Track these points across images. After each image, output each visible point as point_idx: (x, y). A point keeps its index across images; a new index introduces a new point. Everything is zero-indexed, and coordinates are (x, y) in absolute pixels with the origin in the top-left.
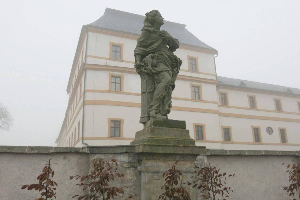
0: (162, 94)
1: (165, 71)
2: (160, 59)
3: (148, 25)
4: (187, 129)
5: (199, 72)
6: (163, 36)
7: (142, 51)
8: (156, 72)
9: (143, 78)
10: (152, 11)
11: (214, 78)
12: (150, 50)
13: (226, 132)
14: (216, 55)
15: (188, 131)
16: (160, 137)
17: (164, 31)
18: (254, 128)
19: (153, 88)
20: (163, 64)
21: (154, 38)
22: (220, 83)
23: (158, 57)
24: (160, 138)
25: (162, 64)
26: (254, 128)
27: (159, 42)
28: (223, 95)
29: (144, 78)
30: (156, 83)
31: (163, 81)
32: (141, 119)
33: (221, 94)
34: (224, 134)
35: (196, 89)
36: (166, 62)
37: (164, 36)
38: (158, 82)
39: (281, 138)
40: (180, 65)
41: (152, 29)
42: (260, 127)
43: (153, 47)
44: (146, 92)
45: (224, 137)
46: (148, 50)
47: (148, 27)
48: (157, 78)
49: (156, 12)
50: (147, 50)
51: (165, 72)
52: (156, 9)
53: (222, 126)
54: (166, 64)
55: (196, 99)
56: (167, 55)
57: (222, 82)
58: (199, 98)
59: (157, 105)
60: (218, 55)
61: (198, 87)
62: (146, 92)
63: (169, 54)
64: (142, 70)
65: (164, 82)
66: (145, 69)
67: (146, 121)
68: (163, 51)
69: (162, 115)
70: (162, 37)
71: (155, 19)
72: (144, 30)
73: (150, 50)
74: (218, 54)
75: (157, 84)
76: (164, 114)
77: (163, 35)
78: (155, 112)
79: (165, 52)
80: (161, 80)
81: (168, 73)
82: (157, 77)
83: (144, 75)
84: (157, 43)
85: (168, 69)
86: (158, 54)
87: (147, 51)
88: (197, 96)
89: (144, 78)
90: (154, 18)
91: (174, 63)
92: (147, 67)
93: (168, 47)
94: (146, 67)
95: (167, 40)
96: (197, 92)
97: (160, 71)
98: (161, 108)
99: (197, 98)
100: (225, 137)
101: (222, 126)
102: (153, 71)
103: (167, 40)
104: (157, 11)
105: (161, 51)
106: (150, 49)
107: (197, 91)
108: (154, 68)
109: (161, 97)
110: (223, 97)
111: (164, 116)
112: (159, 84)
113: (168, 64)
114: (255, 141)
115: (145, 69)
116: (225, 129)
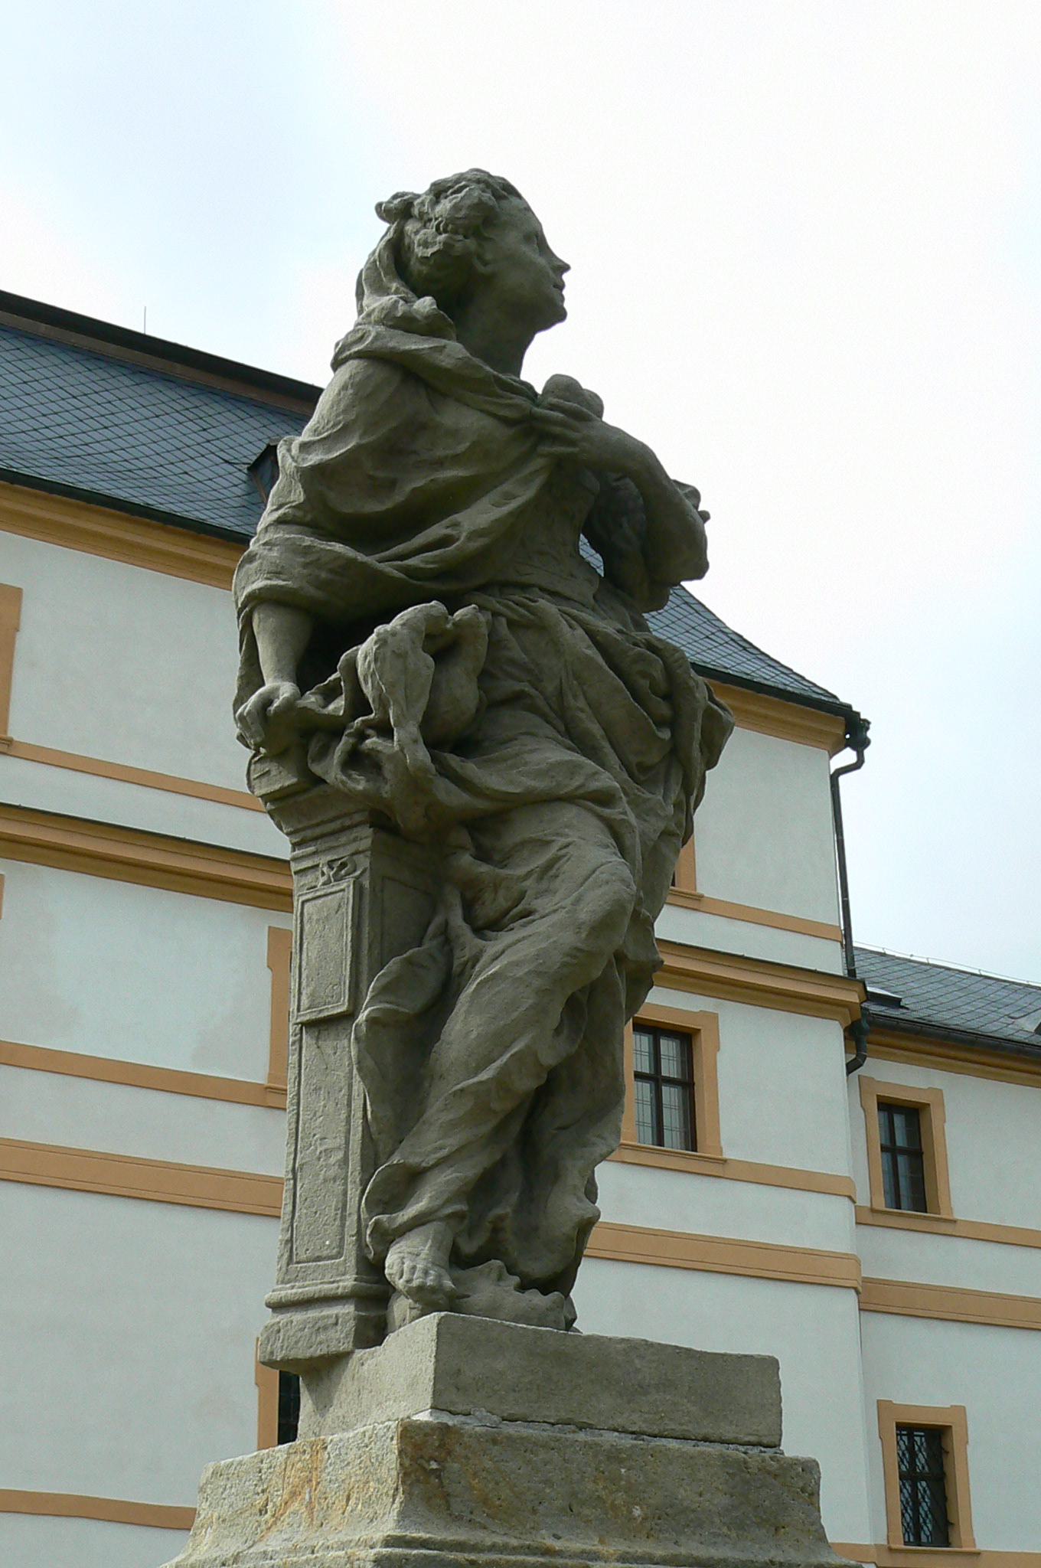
0: (527, 1047)
1: (570, 799)
2: (512, 677)
3: (402, 308)
4: (791, 1448)
5: (699, 898)
6: (558, 430)
7: (324, 575)
8: (482, 804)
9: (323, 860)
10: (460, 178)
11: (829, 959)
12: (409, 571)
13: (921, 1459)
14: (848, 756)
15: (809, 1468)
16: (514, 1542)
17: (564, 388)
18: (906, 1429)
19: (432, 980)
20: (549, 730)
21: (462, 448)
22: (874, 1008)
23: (495, 643)
24: (504, 1549)
25: (538, 720)
26: (900, 1427)
27: (509, 497)
28: (899, 1121)
29: (330, 864)
30: (468, 917)
31: (541, 904)
32: (283, 1318)
33: (888, 1107)
34: (896, 1482)
35: (669, 1048)
36: (581, 703)
37: (574, 435)
38: (489, 908)
39: (949, 1495)
40: (711, 763)
41: (452, 352)
42: (961, 1411)
43: (444, 542)
44: (349, 1016)
45: (898, 1508)
46: (387, 568)
47: (407, 324)
48: (484, 868)
49: (498, 197)
50: (383, 566)
51: (570, 814)
52: (496, 169)
53: (883, 1407)
54: (567, 729)
55: (660, 1141)
56: (591, 634)
57: (895, 1003)
58: (691, 1141)
59: (467, 1171)
60: (867, 752)
61: (686, 1037)
62: (349, 1016)
63: (608, 627)
64: (317, 769)
65: (555, 917)
66: (356, 760)
67: (339, 1339)
68: (542, 589)
69: (522, 1288)
70: (545, 449)
71: (480, 257)
72: (359, 355)
73: (413, 562)
74: (866, 743)
75: (479, 931)
76: (539, 1268)
77: (556, 423)
78: (448, 1243)
79: (567, 599)
80: (522, 896)
81: (601, 818)
82: (483, 855)
83: (333, 833)
84: (484, 503)
85: (606, 781)
86: (495, 614)
87: (376, 576)
88: (672, 1118)
89: (330, 864)
90: (471, 244)
91: (660, 723)
92: (372, 742)
93: (596, 560)
94: (361, 736)
95: (593, 483)
96: (670, 1081)
97: (511, 789)
98: (505, 1209)
99: (673, 1136)
100: (911, 1504)
101: (883, 1407)
102: (449, 795)
103: (593, 483)
104: (504, 191)
105: (524, 587)
106: (413, 562)
107: (670, 1068)
108: (453, 760)
109: (526, 1084)
110: (901, 1141)
111: (545, 1293)
112: (506, 938)
113: (596, 729)
114: (899, 1531)
115: (356, 760)
116: (911, 1437)
